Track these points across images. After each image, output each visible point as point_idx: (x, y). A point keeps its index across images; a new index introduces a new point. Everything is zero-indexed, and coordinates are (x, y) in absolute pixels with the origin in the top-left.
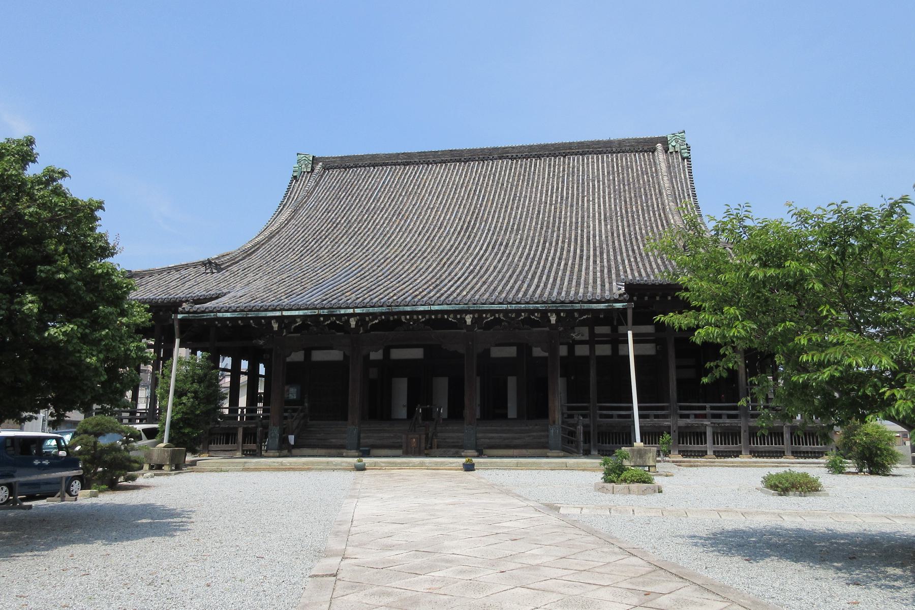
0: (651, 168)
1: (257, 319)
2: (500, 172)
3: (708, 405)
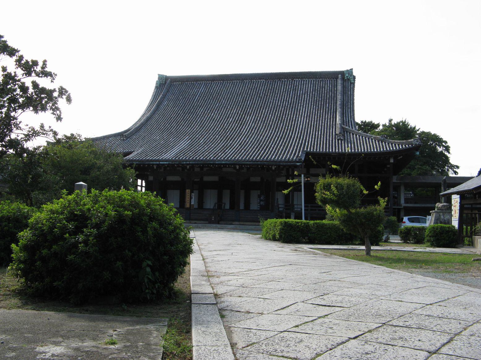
0: (334, 88)
1: (149, 165)
2: (260, 87)
3: (309, 205)
